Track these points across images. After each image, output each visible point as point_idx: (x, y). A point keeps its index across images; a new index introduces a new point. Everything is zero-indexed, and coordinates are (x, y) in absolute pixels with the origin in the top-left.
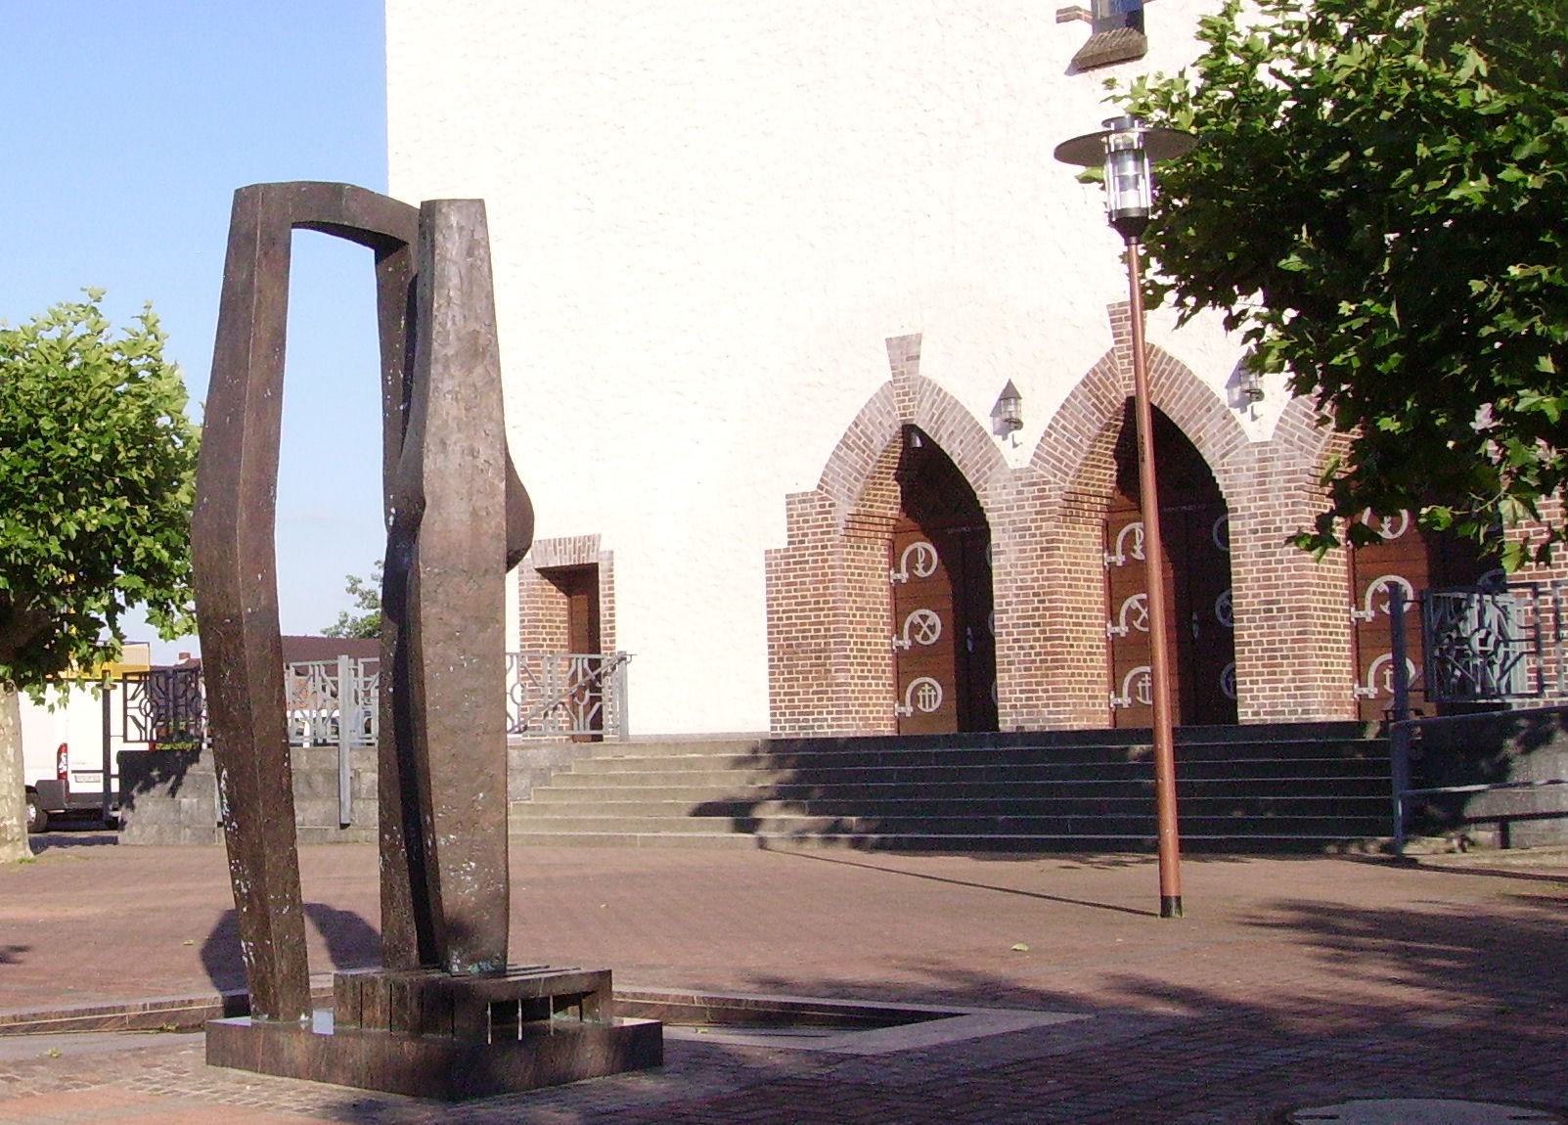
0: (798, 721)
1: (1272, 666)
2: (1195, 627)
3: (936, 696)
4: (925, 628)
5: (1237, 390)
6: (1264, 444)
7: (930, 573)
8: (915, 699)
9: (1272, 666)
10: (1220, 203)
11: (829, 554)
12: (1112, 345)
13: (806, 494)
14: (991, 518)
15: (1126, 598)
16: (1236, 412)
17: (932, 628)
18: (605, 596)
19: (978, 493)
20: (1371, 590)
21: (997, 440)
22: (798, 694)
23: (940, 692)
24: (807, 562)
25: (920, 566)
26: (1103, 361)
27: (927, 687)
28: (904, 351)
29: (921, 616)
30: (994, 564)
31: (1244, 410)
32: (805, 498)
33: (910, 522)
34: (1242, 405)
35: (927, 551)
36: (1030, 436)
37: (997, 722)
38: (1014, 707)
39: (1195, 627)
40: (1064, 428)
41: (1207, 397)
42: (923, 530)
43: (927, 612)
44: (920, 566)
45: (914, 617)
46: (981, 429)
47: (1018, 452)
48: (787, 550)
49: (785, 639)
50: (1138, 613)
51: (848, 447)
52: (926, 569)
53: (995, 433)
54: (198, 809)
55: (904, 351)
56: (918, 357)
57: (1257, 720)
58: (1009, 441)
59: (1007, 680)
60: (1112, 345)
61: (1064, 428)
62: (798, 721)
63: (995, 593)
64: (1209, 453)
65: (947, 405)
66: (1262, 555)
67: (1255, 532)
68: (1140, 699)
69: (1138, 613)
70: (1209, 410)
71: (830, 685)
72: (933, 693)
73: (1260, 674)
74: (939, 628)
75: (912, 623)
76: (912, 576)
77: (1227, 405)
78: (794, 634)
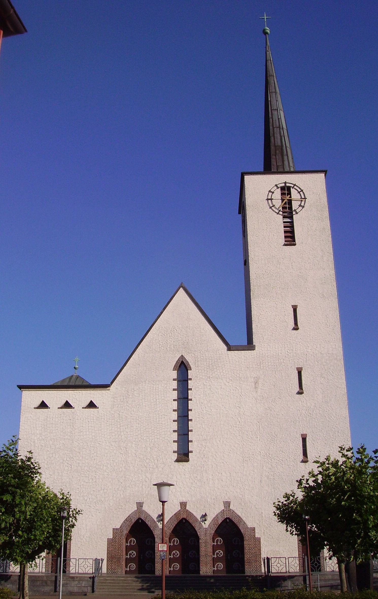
0: (113, 571)
1: (206, 565)
2: (185, 557)
3: (134, 567)
4: (220, 554)
5: (202, 519)
6: (206, 528)
7: (177, 544)
8: (130, 567)
9: (206, 565)
10: (23, 492)
11: (122, 540)
12: (180, 509)
13: (117, 528)
14: (156, 536)
15: (130, 551)
16: (202, 522)
17: (221, 554)
18: (68, 544)
19: (153, 532)
20: (173, 553)
21: (157, 523)
22: (113, 566)
23: (222, 565)
24: (117, 541)
25: (132, 543)
26: (178, 511)
27: (220, 565)
28: (140, 505)
29: (132, 552)
30: (156, 544)
31: (203, 522)
32: (117, 529)
33: (173, 535)
34: (203, 521)
35: (134, 540)
36: (207, 523)
37: (155, 573)
38: (158, 570)
39: (185, 557)
40: (170, 522)
41: (197, 519)
42: (133, 536)
43: (220, 551)
44: (132, 543)
45: (131, 552)
46: (154, 520)
47: (206, 525)
48: (112, 539)
49: (111, 555)
50: (218, 553)
51: (127, 521)
52: (133, 543)
53: (157, 521)
54: (12, 588)
55: (140, 505)
56: (142, 506)
57: (205, 574)
58: (204, 523)
59: (157, 565)
60: (180, 509)
61: (170, 522)
62: (113, 571)
63: (156, 550)
64: (197, 529)
65: (148, 516)
66: (205, 546)
67: (204, 542)
68: (175, 569)
69: (218, 553)
70: (197, 522)
71: (120, 564)
72: (177, 566)
73: (204, 566)
74: (135, 554)
75: (217, 553)
76: (174, 545)
77: (156, 521)
78: (113, 555)
